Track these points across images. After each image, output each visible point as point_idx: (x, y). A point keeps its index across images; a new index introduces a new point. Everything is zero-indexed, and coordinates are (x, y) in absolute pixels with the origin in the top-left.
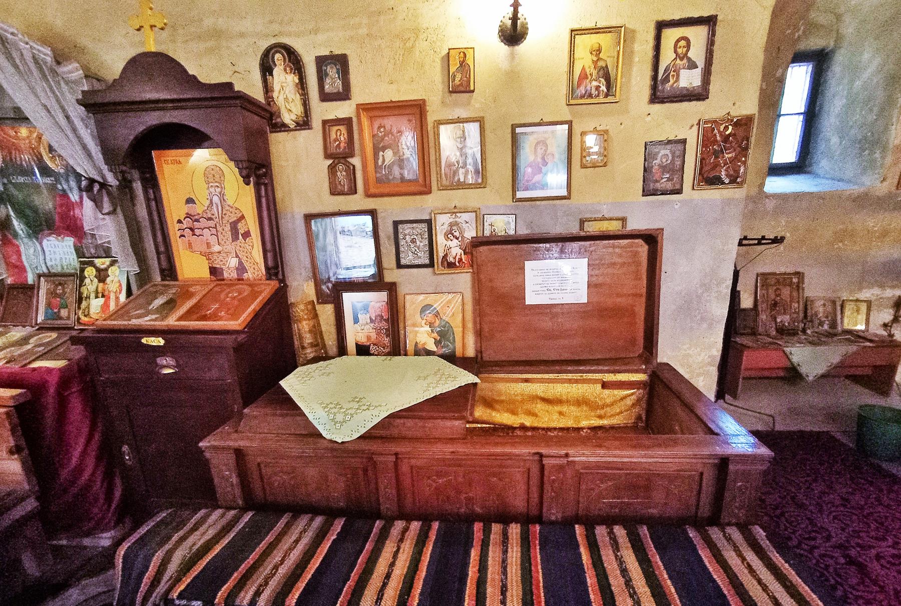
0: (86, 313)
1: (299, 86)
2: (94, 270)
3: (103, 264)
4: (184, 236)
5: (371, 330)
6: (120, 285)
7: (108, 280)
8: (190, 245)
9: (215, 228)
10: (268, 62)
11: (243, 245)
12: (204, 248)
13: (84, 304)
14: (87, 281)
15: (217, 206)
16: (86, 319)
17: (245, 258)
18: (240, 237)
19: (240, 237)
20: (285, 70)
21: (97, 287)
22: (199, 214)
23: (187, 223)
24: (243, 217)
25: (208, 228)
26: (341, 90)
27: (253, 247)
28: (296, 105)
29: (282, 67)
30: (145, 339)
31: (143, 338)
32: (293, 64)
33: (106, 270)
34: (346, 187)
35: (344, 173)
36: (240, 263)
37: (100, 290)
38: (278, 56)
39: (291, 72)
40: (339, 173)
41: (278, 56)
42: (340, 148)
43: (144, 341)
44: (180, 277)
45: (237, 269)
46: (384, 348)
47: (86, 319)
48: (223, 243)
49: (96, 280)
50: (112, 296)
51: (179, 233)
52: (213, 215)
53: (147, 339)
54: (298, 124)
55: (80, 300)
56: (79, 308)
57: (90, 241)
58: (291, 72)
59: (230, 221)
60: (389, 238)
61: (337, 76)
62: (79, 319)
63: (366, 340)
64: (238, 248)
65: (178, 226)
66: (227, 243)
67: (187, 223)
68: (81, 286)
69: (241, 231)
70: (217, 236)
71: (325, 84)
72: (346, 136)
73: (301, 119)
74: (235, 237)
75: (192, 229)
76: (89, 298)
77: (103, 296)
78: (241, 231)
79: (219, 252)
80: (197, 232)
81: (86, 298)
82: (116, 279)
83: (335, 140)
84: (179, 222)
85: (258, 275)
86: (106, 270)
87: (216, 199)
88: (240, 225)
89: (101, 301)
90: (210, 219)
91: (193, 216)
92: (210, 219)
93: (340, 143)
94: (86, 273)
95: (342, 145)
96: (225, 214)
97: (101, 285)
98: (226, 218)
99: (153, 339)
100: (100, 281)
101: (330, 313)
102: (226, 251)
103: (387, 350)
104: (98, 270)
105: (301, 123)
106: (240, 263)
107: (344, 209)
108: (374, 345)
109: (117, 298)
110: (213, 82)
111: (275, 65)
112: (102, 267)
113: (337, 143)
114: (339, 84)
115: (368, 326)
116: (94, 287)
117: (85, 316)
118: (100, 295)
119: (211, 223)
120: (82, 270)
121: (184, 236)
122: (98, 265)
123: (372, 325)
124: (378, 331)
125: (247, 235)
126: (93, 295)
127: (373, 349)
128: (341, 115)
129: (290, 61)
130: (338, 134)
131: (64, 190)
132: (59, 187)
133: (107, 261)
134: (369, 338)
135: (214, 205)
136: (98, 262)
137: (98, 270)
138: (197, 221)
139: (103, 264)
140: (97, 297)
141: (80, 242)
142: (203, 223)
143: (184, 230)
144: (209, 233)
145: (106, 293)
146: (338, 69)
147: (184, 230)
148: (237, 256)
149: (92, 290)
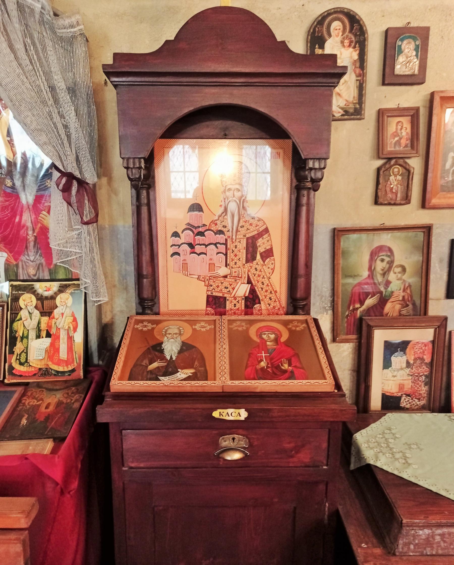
0: (23, 360)
1: (358, 65)
2: (34, 298)
3: (48, 290)
4: (179, 254)
5: (406, 377)
6: (75, 320)
7: (56, 312)
8: (185, 267)
9: (226, 244)
10: (321, 31)
11: (259, 268)
12: (205, 272)
13: (19, 347)
14: (23, 314)
15: (233, 216)
16: (23, 369)
17: (260, 285)
18: (258, 257)
19: (258, 257)
20: (342, 42)
21: (39, 323)
22: (204, 225)
23: (187, 236)
24: (266, 231)
25: (215, 244)
26: (416, 72)
27: (273, 270)
28: (348, 88)
29: (339, 39)
30: (242, 418)
31: (216, 409)
32: (355, 35)
33: (53, 298)
34: (399, 195)
35: (399, 178)
36: (253, 291)
37: (43, 326)
38: (336, 25)
39: (350, 46)
40: (392, 178)
41: (336, 25)
42: (400, 146)
43: (216, 414)
44: (163, 309)
45: (246, 299)
46: (419, 399)
47: (23, 369)
48: (232, 264)
49: (37, 313)
50: (63, 336)
51: (171, 251)
52: (225, 227)
53: (221, 411)
54: (346, 112)
55: (13, 341)
56: (12, 352)
57: (32, 258)
58: (350, 46)
59: (248, 236)
60: (441, 261)
61: (414, 53)
62: (11, 368)
63: (397, 390)
64: (253, 271)
65: (172, 240)
66: (239, 264)
67: (187, 236)
68: (13, 321)
69: (261, 249)
70: (226, 255)
71: (397, 62)
72: (409, 130)
73: (352, 106)
74: (251, 257)
75: (191, 246)
76: (27, 337)
77: (48, 335)
78: (261, 249)
79: (225, 277)
80: (198, 249)
81: (22, 338)
82: (68, 312)
83: (395, 134)
84: (176, 234)
85: (274, 307)
86: (53, 298)
87: (232, 207)
88: (260, 242)
89: (46, 342)
90: (221, 232)
91: (196, 228)
92: (221, 232)
93: (401, 139)
94: (22, 303)
95: (403, 142)
96: (242, 227)
97: (45, 320)
98: (243, 231)
99: (230, 411)
100: (43, 314)
101: (346, 353)
102: (234, 274)
103: (423, 402)
104: (40, 298)
105: (351, 111)
106: (253, 291)
107: (389, 223)
108: (408, 395)
109: (70, 339)
110: (147, 52)
111: (330, 35)
112: (46, 294)
113: (397, 139)
114: (416, 63)
115: (401, 372)
116: (34, 323)
117: (21, 364)
118: (44, 334)
119: (221, 238)
120: (16, 299)
121: (179, 254)
122: (40, 291)
123: (408, 370)
124: (415, 377)
125: (268, 254)
126: (32, 334)
127: (404, 403)
128: (405, 104)
129: (351, 31)
130: (399, 127)
131: (13, 187)
132: (9, 183)
133: (55, 286)
134: (401, 387)
135: (229, 214)
136: (40, 287)
137: (40, 298)
138: (201, 234)
139: (48, 290)
140: (38, 336)
141: (16, 260)
142: (210, 237)
143: (179, 246)
144: (216, 250)
145: (53, 331)
146: (417, 47)
147: (179, 246)
148: (249, 282)
149: (31, 326)
